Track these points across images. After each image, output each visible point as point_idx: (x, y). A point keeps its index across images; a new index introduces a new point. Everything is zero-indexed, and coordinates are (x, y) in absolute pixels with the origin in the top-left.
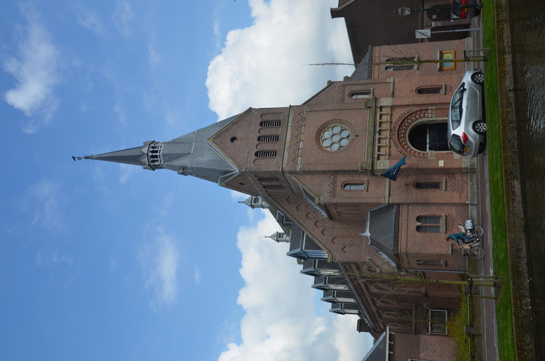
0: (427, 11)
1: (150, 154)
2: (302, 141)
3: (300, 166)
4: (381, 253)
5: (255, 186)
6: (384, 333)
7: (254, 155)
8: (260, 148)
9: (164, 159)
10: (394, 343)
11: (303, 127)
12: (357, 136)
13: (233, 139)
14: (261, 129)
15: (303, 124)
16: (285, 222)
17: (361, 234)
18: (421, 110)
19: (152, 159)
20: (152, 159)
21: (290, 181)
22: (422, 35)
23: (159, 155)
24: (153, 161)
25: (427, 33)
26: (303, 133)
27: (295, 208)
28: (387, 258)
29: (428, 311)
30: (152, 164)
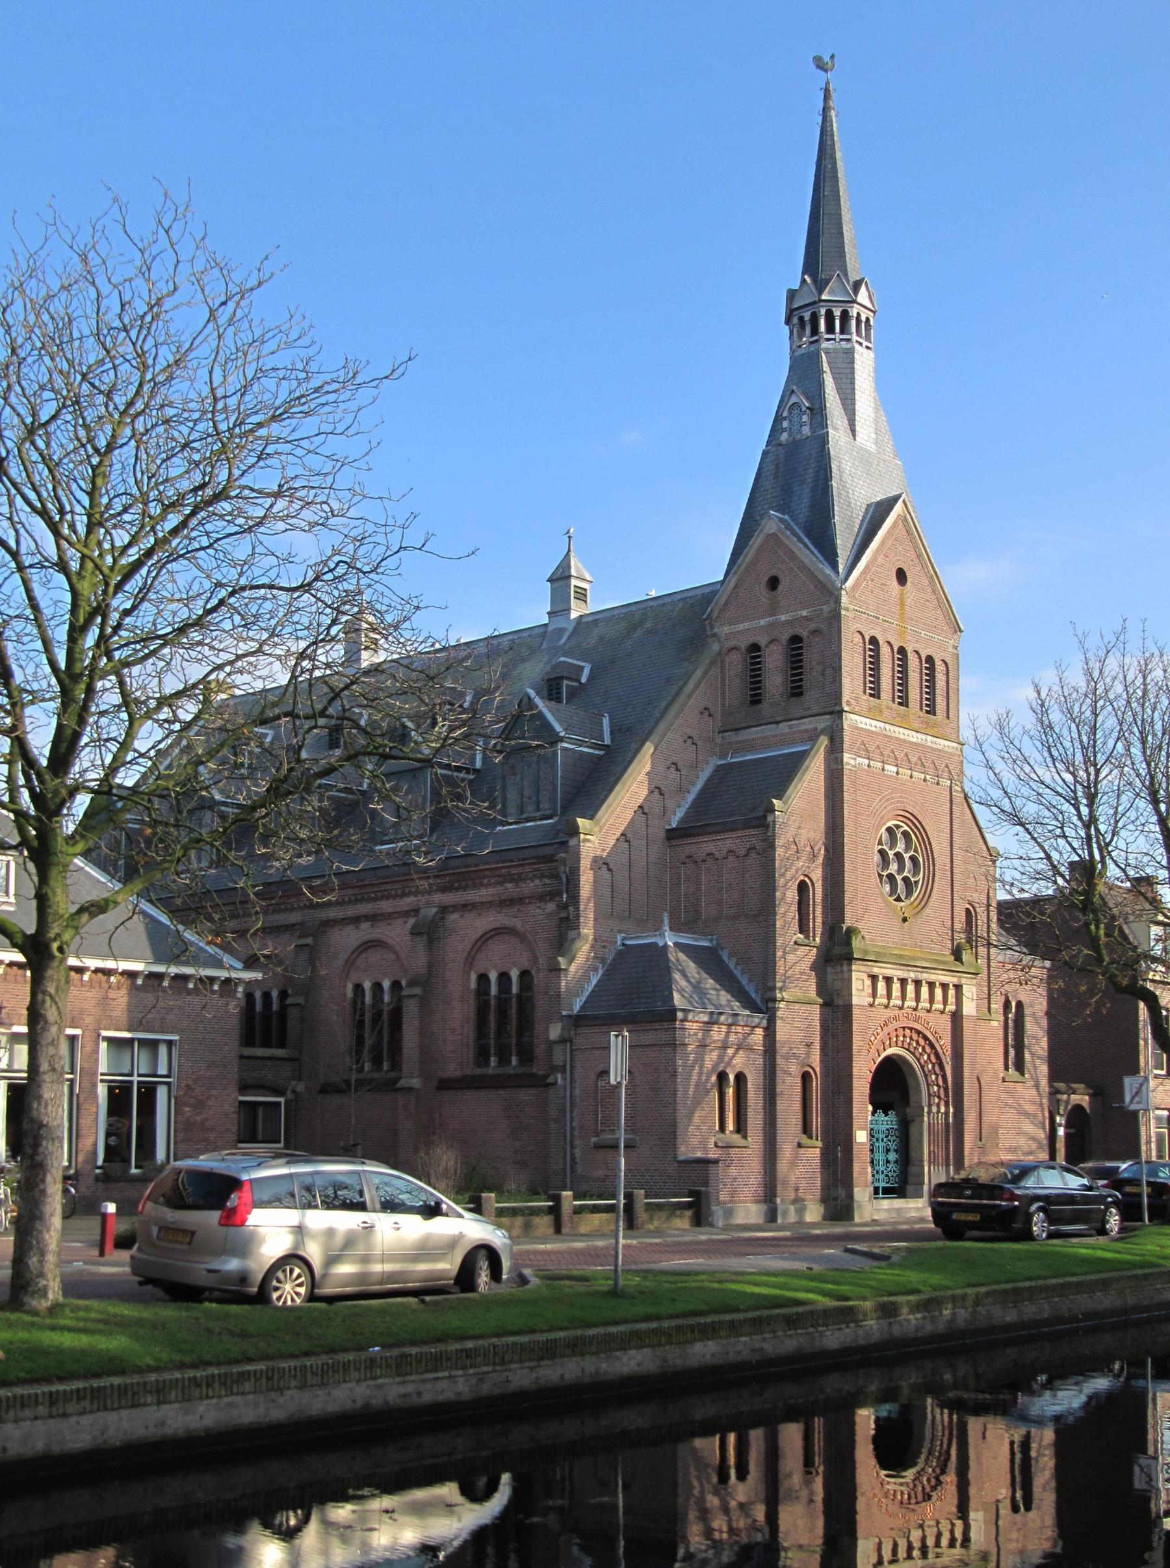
0: (398, 1085)
1: (854, 312)
2: (897, 773)
3: (852, 762)
4: (600, 972)
5: (762, 622)
6: (239, 965)
7: (873, 633)
8: (885, 650)
9: (835, 351)
10: (189, 992)
11: (923, 776)
12: (905, 920)
13: (901, 576)
14: (920, 657)
15: (928, 777)
16: (567, 686)
17: (666, 921)
18: (946, 1089)
19: (837, 313)
20: (837, 313)
21: (790, 727)
22: (1134, 1090)
23: (849, 340)
24: (830, 317)
25: (1138, 1103)
26: (911, 777)
27: (689, 731)
28: (590, 989)
29: (281, 1093)
30: (823, 311)
